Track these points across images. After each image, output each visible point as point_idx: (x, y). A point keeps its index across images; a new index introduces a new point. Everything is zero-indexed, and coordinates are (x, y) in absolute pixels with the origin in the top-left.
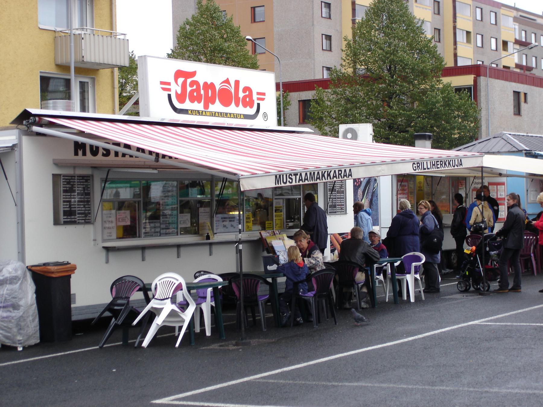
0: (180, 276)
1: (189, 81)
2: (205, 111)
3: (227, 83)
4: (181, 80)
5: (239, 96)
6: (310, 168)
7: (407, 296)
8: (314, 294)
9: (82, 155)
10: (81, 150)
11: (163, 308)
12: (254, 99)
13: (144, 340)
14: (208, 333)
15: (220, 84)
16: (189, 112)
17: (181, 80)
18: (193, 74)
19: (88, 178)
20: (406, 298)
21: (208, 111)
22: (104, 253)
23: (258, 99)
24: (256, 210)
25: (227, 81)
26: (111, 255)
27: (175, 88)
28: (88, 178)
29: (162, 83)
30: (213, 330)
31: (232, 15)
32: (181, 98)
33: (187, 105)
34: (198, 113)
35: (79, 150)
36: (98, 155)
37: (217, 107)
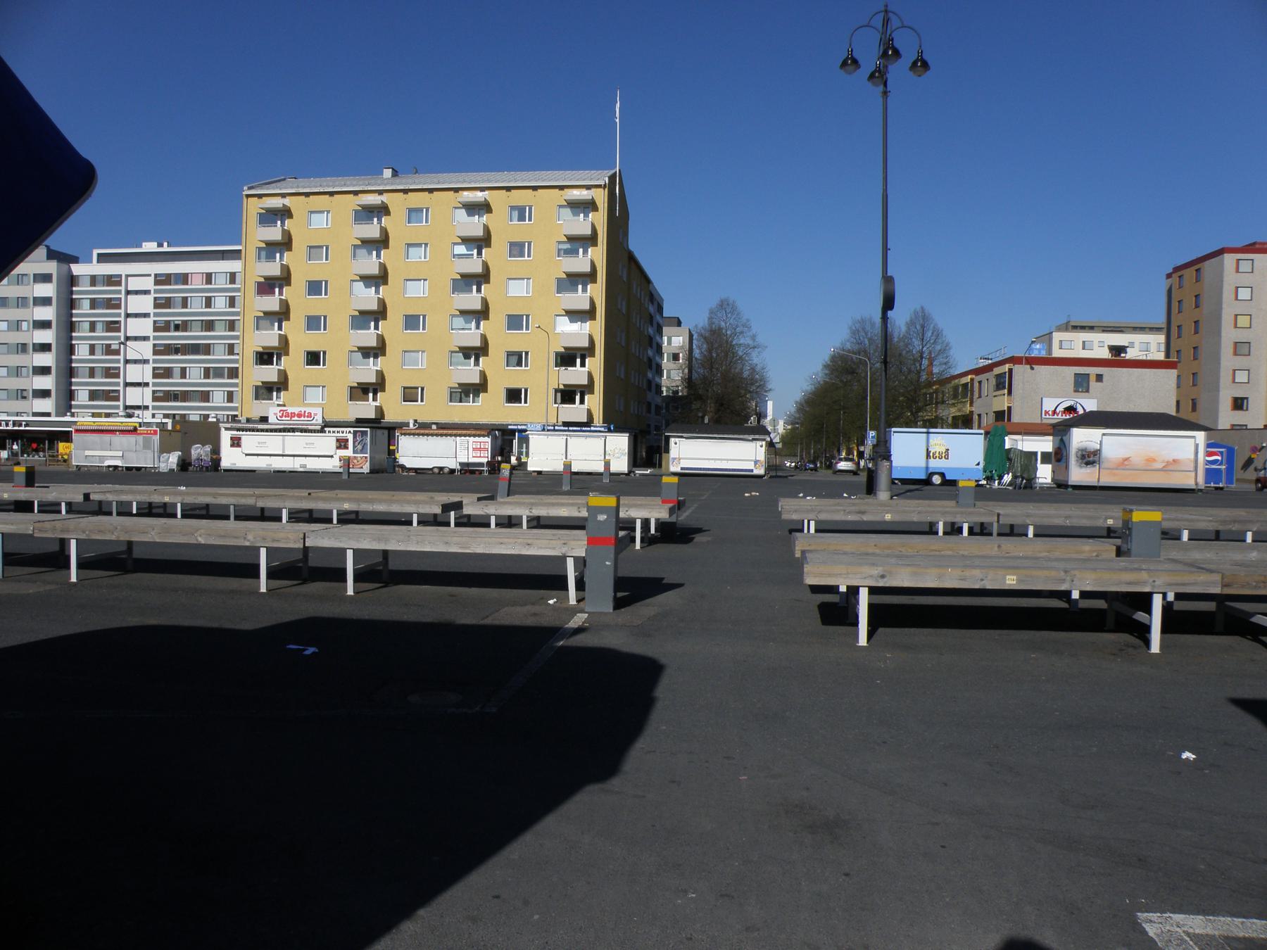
33: (284, 418)
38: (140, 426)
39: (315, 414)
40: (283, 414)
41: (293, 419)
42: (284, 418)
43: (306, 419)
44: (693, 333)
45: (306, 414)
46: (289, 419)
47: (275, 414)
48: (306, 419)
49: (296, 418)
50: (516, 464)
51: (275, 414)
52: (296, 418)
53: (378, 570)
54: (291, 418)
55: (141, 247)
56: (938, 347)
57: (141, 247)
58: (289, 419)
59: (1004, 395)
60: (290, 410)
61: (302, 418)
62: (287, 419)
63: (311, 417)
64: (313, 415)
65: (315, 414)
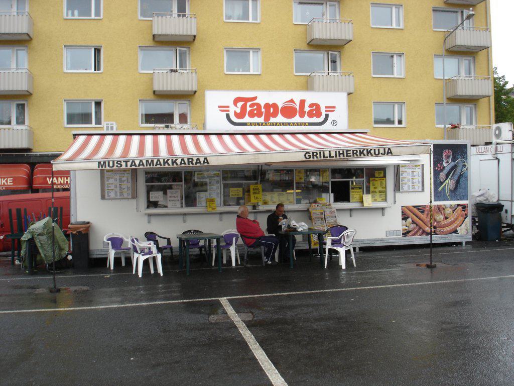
4: (240, 104)
6: (357, 146)
7: (136, 272)
13: (449, 200)
17: (240, 104)
18: (255, 98)
19: (338, 153)
20: (152, 272)
22: (146, 218)
23: (326, 111)
24: (34, 212)
25: (292, 101)
26: (152, 218)
27: (233, 109)
28: (338, 153)
30: (143, 274)
31: (334, 62)
32: (239, 115)
33: (247, 119)
37: (280, 118)
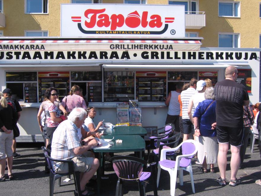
0: (53, 134)
1: (98, 15)
2: (112, 31)
3: (136, 14)
4: (90, 15)
5: (147, 21)
8: (75, 184)
9: (151, 58)
10: (50, 56)
11: (203, 144)
12: (162, 21)
14: (102, 178)
15: (128, 15)
16: (97, 32)
17: (90, 15)
18: (104, 10)
21: (115, 31)
29: (72, 18)
33: (96, 28)
34: (109, 33)
35: (48, 56)
36: (4, 58)
38: (161, 97)
39: (170, 20)
40: (93, 18)
41: (118, 29)
42: (96, 28)
43: (148, 28)
44: (107, 128)
45: (149, 20)
46: (109, 29)
47: (76, 19)
48: (148, 28)
49: (125, 27)
50: (110, 133)
51: (76, 19)
52: (125, 27)
53: (14, 102)
54: (113, 28)
55: (110, 22)
56: (67, 139)
57: (110, 22)
58: (109, 29)
59: (127, 115)
60: (111, 10)
61: (140, 28)
62: (104, 28)
63: (159, 25)
64: (163, 21)
65: (170, 20)
